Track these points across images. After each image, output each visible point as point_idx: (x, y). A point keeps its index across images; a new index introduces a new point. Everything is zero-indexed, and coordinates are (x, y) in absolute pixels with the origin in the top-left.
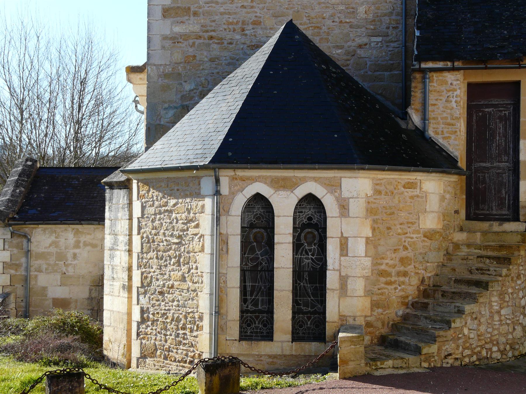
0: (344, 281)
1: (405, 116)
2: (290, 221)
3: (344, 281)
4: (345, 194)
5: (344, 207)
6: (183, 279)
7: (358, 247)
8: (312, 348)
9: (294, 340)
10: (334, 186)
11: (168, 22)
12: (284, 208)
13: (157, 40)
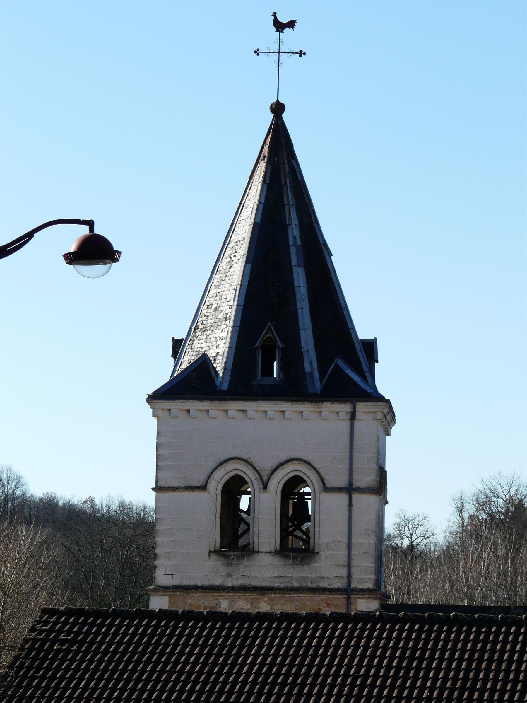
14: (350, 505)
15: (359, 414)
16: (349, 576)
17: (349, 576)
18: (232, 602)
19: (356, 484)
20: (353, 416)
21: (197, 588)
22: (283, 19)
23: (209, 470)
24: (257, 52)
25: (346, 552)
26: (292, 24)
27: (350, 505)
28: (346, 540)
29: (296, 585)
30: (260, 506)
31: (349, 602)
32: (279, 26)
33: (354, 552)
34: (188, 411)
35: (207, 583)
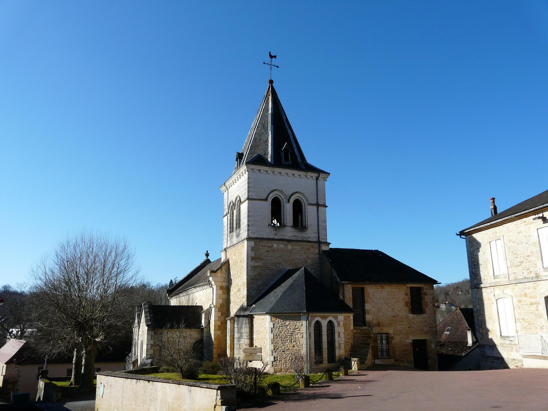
0: (339, 344)
1: (339, 296)
2: (326, 328)
3: (339, 344)
4: (339, 320)
5: (339, 324)
6: (294, 346)
7: (342, 335)
8: (333, 365)
9: (328, 363)
10: (336, 318)
11: (253, 262)
12: (324, 324)
13: (250, 267)
14: (318, 210)
15: (320, 178)
16: (319, 237)
17: (319, 237)
18: (278, 245)
19: (319, 203)
20: (317, 178)
21: (265, 239)
22: (273, 55)
23: (268, 194)
24: (264, 63)
25: (317, 228)
26: (275, 57)
27: (318, 210)
28: (538, 241)
29: (300, 239)
30: (288, 209)
31: (319, 247)
32: (271, 57)
33: (320, 228)
34: (260, 170)
35: (268, 237)
